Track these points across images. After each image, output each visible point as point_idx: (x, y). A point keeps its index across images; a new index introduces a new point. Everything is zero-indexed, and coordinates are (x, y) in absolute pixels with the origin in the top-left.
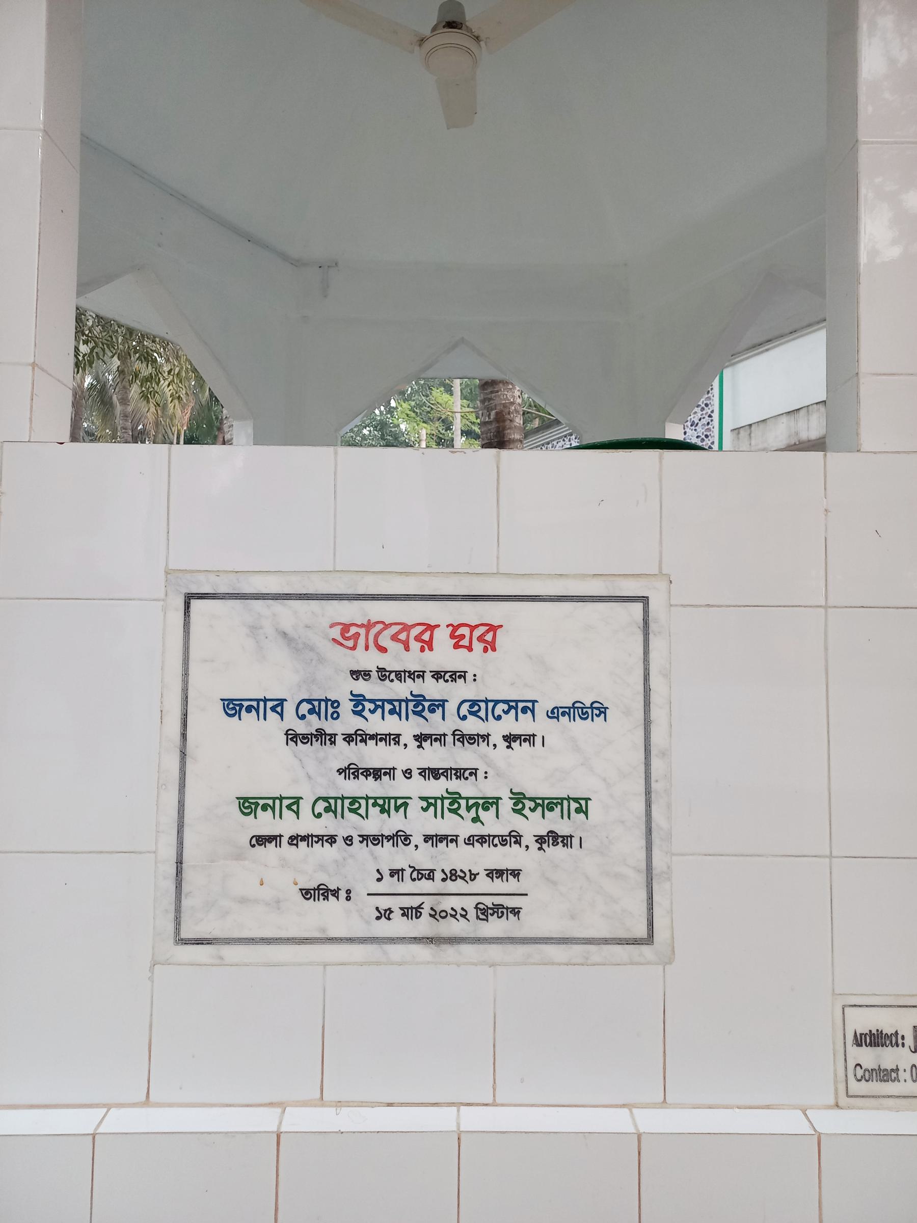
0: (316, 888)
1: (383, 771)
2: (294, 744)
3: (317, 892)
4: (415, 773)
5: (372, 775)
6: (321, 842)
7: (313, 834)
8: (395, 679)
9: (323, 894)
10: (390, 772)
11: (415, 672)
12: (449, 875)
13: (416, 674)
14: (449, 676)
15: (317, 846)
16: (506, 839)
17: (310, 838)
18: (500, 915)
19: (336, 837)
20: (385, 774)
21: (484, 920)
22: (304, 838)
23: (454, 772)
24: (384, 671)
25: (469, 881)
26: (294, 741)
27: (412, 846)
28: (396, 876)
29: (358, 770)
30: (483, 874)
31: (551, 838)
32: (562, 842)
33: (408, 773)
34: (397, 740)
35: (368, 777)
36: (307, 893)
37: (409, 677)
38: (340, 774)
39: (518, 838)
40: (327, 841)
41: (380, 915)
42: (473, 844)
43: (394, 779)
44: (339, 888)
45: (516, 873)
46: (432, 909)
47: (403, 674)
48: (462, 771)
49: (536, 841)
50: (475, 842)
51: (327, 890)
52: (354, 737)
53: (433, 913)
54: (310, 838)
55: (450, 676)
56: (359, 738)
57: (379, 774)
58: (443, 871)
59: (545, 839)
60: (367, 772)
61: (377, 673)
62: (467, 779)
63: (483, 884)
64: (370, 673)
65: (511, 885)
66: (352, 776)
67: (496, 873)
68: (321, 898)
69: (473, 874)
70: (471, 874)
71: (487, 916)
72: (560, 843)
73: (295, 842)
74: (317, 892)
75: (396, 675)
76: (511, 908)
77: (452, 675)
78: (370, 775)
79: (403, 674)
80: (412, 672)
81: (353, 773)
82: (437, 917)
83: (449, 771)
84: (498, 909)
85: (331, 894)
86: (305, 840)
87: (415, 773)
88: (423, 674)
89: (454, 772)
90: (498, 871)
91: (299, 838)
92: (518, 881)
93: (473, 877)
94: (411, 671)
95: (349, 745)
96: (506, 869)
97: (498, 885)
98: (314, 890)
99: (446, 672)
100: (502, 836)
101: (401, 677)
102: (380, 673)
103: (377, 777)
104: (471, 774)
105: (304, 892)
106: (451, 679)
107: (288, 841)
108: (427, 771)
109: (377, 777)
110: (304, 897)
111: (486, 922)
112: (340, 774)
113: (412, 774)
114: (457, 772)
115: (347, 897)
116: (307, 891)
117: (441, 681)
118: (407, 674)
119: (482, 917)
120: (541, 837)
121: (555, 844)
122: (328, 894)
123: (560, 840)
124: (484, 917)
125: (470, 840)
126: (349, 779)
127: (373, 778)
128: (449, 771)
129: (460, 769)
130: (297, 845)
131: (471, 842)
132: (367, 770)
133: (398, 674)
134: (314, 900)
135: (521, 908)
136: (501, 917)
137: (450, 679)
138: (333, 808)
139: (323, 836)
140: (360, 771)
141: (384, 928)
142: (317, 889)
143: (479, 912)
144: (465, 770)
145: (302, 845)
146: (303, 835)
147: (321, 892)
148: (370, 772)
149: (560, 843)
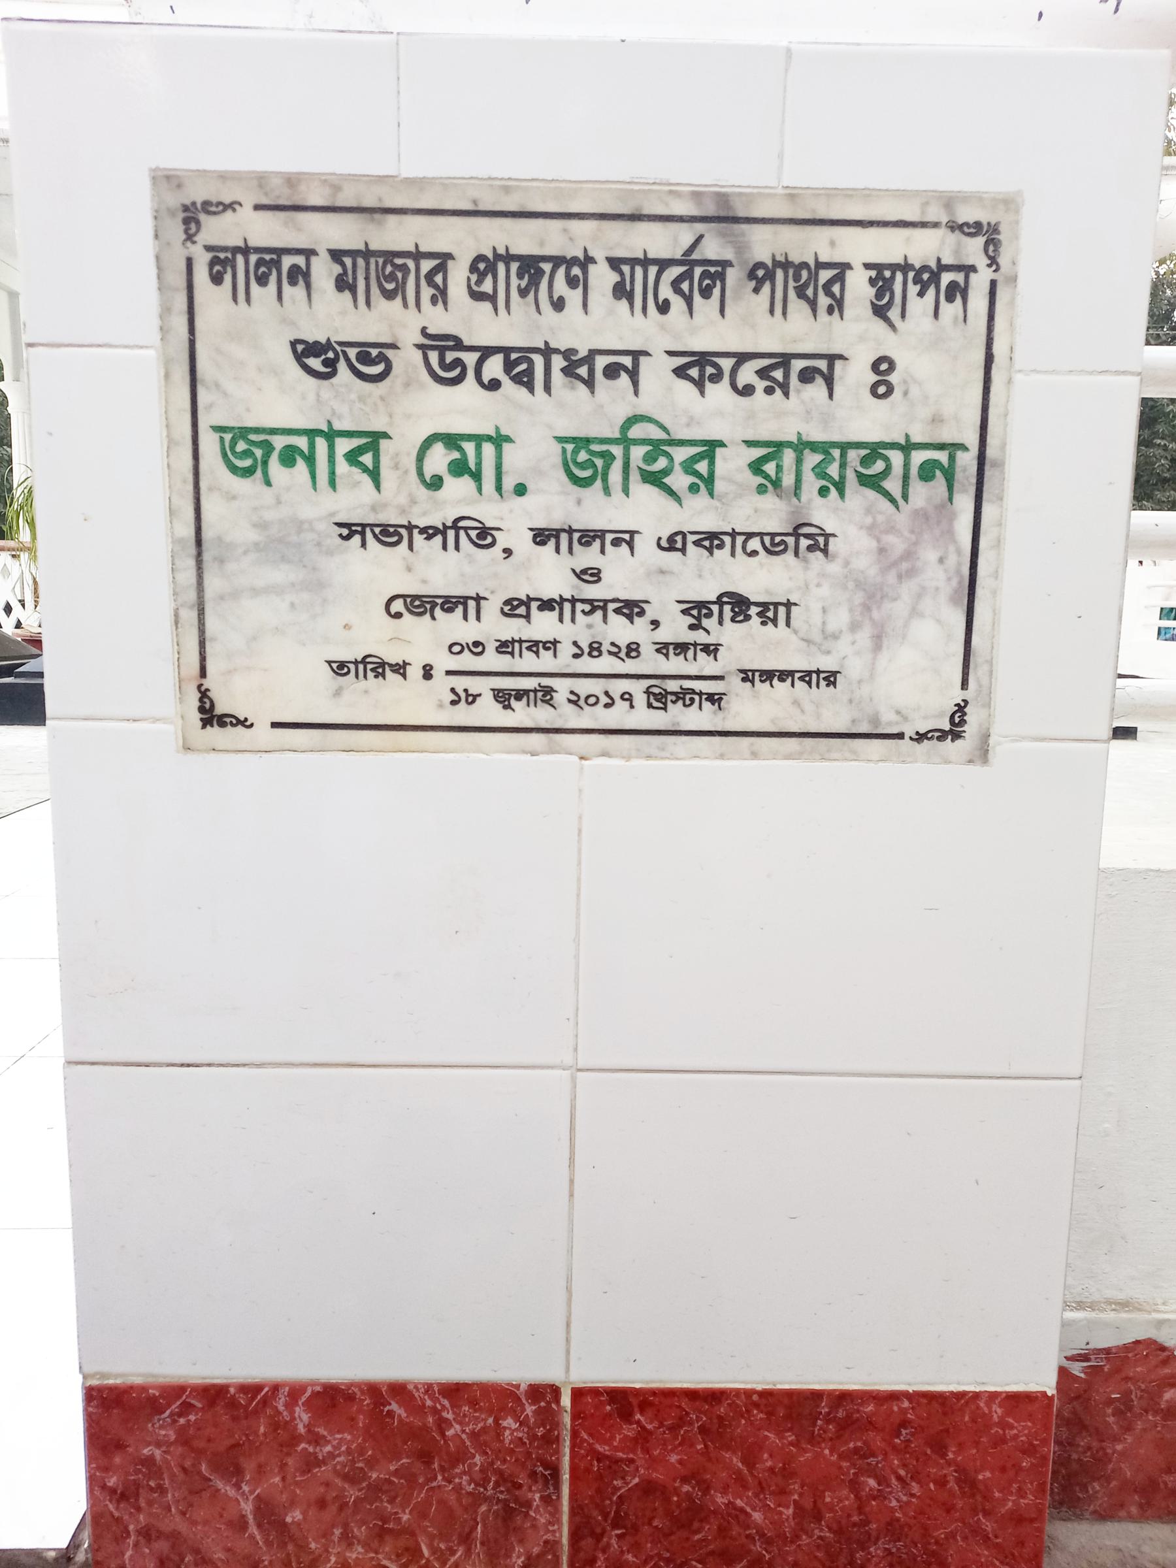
3: (361, 667)
11: (593, 353)
12: (587, 650)
13: (601, 362)
18: (688, 702)
19: (643, 605)
21: (661, 708)
25: (625, 658)
28: (525, 699)
31: (727, 608)
32: (759, 614)
41: (456, 699)
44: (407, 661)
46: (572, 692)
47: (538, 360)
51: (383, 664)
52: (790, 540)
53: (574, 698)
55: (763, 373)
56: (804, 543)
58: (575, 643)
63: (492, 660)
64: (390, 353)
65: (704, 664)
67: (675, 649)
68: (370, 674)
71: (665, 704)
74: (361, 667)
75: (509, 366)
76: (706, 694)
77: (772, 367)
79: (538, 360)
80: (583, 353)
82: (582, 703)
84: (685, 694)
91: (534, 605)
92: (716, 660)
96: (693, 643)
97: (675, 665)
98: (356, 663)
99: (742, 358)
101: (530, 372)
102: (434, 357)
105: (335, 666)
107: (502, 609)
111: (663, 711)
116: (342, 665)
118: (558, 362)
119: (656, 704)
120: (701, 605)
123: (754, 610)
130: (527, 617)
133: (517, 362)
134: (357, 676)
135: (724, 694)
136: (690, 705)
137: (760, 385)
138: (751, 678)
139: (606, 602)
141: (463, 715)
143: (652, 697)
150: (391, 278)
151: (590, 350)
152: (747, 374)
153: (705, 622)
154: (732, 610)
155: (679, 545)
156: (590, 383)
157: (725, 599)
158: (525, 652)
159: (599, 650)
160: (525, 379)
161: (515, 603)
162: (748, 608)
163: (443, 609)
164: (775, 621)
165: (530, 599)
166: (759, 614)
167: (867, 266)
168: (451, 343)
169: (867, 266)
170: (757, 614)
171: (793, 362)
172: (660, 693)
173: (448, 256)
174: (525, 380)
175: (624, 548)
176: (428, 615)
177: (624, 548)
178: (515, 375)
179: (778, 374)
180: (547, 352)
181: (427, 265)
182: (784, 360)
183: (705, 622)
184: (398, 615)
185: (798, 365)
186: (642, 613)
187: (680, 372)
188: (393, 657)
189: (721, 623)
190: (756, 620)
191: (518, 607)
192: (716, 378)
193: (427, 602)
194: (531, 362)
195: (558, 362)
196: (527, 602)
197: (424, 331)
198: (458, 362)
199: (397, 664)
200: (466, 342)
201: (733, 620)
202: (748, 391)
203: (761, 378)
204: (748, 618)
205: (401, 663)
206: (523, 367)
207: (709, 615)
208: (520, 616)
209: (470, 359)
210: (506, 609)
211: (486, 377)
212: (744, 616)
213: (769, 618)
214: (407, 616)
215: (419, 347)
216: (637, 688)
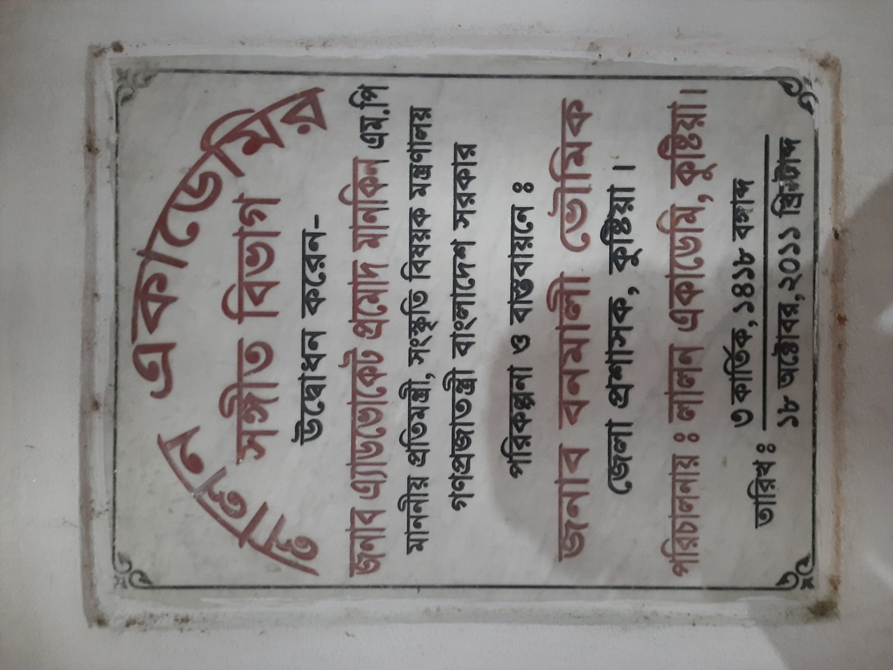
1: (515, 390)
2: (426, 267)
7: (607, 349)
8: (317, 401)
9: (765, 489)
12: (743, 299)
13: (308, 351)
15: (632, 340)
16: (682, 240)
20: (521, 386)
22: (615, 373)
24: (303, 427)
26: (422, 267)
27: (630, 301)
29: (513, 439)
30: (740, 243)
31: (616, 237)
32: (622, 211)
34: (421, 113)
36: (763, 517)
37: (314, 367)
38: (520, 472)
39: (678, 213)
42: (695, 313)
43: (530, 369)
49: (687, 183)
50: (688, 307)
51: (759, 482)
54: (616, 357)
55: (313, 269)
57: (522, 397)
62: (530, 226)
66: (525, 449)
67: (740, 221)
68: (770, 491)
70: (786, 409)
72: (692, 131)
73: (621, 392)
75: (311, 398)
78: (522, 415)
80: (304, 360)
83: (516, 260)
86: (619, 369)
90: (736, 219)
91: (615, 381)
93: (746, 259)
94: (303, 365)
95: (429, 216)
99: (305, 280)
100: (673, 248)
101: (314, 387)
102: (306, 436)
104: (522, 218)
105: (760, 521)
106: (318, 267)
108: (516, 306)
112: (520, 472)
113: (520, 334)
115: (769, 450)
116: (759, 515)
117: (323, 291)
118: (309, 373)
123: (618, 216)
125: (683, 318)
127: (528, 408)
128: (516, 260)
129: (513, 237)
130: (628, 388)
131: (689, 316)
132: (513, 421)
134: (774, 503)
137: (319, 270)
144: (514, 228)
145: (628, 375)
147: (761, 492)
148: (518, 414)
149: (692, 131)
150: (367, 565)
152: (314, 277)
154: (618, 233)
155: (157, 357)
157: (608, 238)
159: (743, 288)
160: (318, 390)
161: (614, 397)
162: (617, 221)
163: (623, 451)
164: (628, 200)
165: (610, 385)
168: (300, 428)
170: (621, 213)
172: (781, 201)
173: (353, 511)
174: (318, 390)
176: (628, 463)
178: (315, 393)
179: (314, 261)
180: (303, 378)
181: (359, 524)
182: (306, 259)
184: (629, 485)
185: (309, 252)
186: (622, 301)
188: (753, 474)
189: (630, 241)
190: (628, 214)
192: (316, 292)
193: (615, 463)
194: (309, 386)
195: (309, 373)
197: (294, 440)
198: (310, 423)
199: (758, 469)
200: (299, 419)
201: (627, 232)
202: (322, 277)
203: (316, 269)
204: (625, 220)
205: (756, 466)
206: (311, 391)
207: (623, 250)
209: (308, 418)
210: (619, 403)
211: (317, 409)
212: (624, 223)
213: (625, 205)
214: (628, 478)
215: (302, 443)
216: (777, 225)
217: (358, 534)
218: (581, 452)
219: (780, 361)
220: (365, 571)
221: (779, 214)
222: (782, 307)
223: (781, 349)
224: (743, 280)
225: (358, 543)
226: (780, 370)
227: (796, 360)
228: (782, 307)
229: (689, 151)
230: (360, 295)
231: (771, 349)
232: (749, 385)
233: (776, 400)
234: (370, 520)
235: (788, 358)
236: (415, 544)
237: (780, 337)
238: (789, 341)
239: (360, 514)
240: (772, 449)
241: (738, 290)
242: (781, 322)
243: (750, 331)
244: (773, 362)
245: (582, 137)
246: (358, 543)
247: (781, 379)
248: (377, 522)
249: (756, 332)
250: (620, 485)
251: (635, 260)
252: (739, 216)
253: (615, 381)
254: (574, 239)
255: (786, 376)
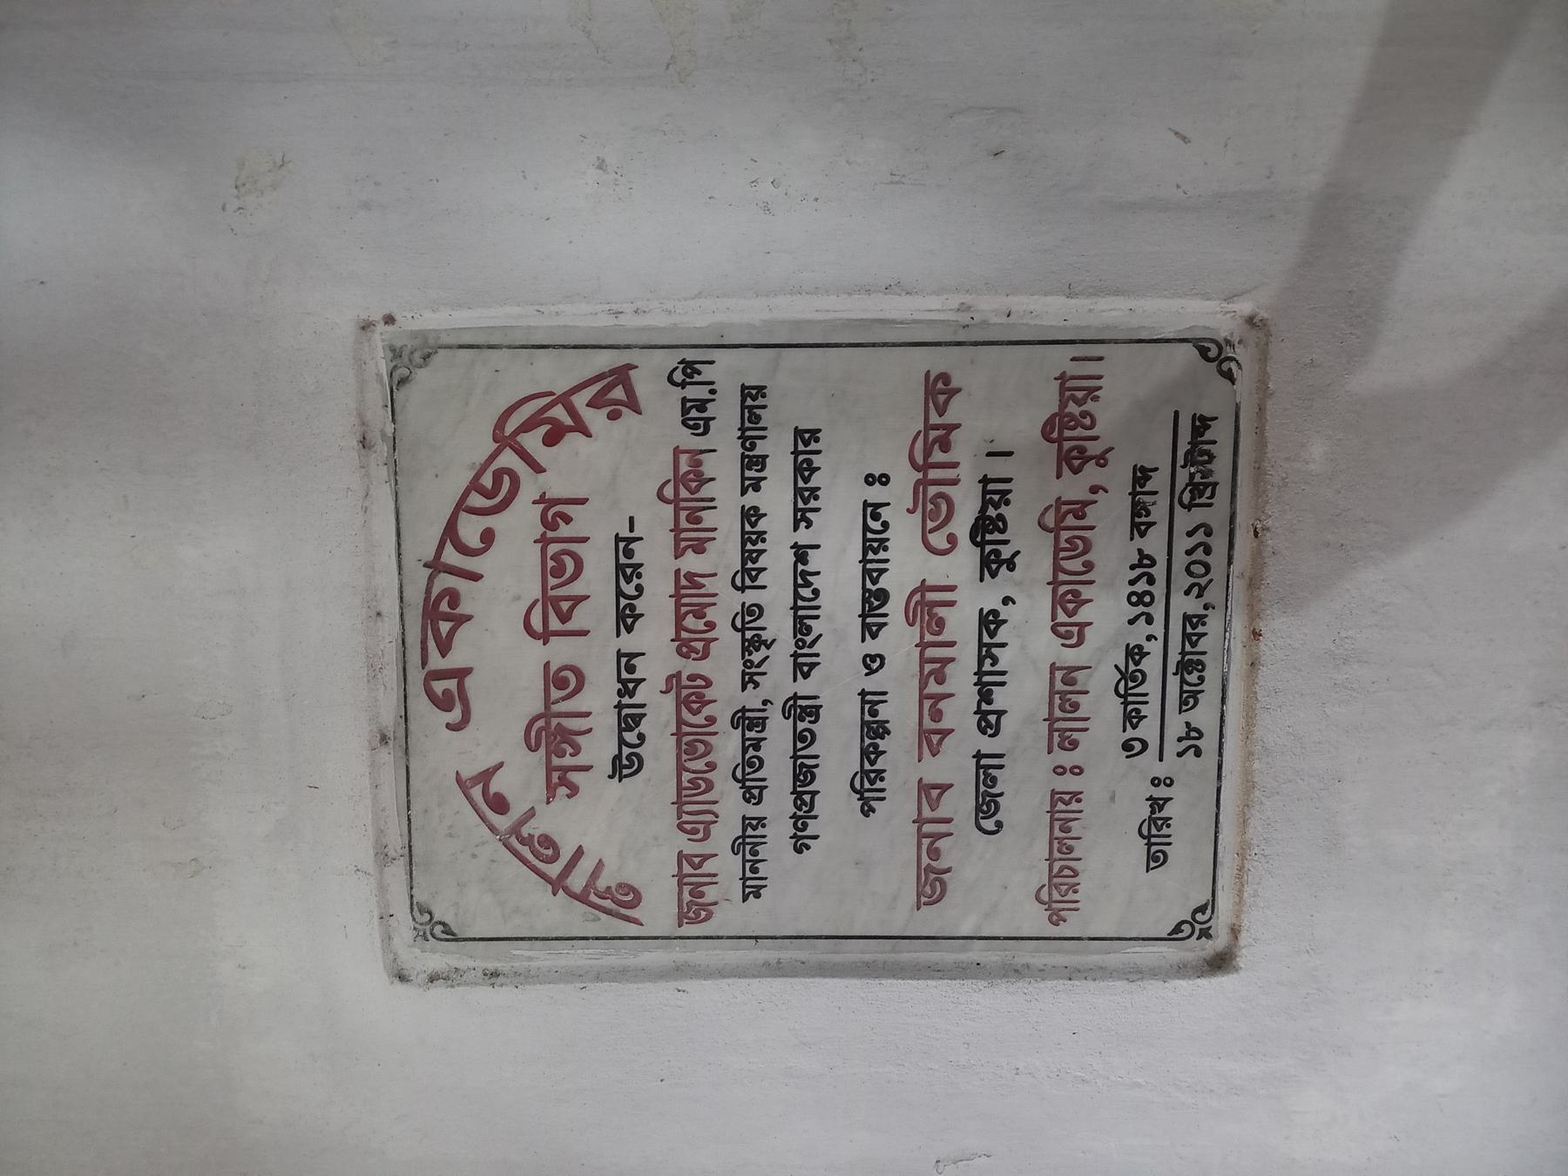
0: (1146, 841)
1: (867, 717)
3: (1153, 840)
4: (872, 647)
5: (878, 741)
6: (994, 650)
10: (870, 702)
11: (619, 680)
12: (1141, 609)
13: (625, 675)
14: (628, 583)
15: (1005, 658)
17: (986, 679)
20: (874, 713)
23: (871, 556)
24: (621, 761)
27: (1005, 613)
31: (988, 537)
32: (996, 507)
33: (873, 663)
35: (814, 465)
36: (1156, 859)
37: (632, 694)
39: (1064, 508)
40: (992, 635)
42: (1082, 626)
43: (885, 693)
45: (1142, 475)
47: (625, 711)
48: (869, 535)
49: (1076, 471)
51: (1152, 820)
53: (1195, 590)
54: (986, 679)
57: (875, 726)
59: (1132, 711)
60: (870, 753)
61: (624, 780)
68: (1165, 831)
69: (1188, 733)
72: (1084, 408)
73: (992, 718)
74: (1153, 840)
77: (625, 575)
78: (876, 746)
79: (625, 711)
80: (620, 686)
81: (872, 782)
83: (869, 566)
85: (1159, 812)
86: (991, 692)
87: (872, 647)
88: (626, 655)
89: (871, 556)
90: (1135, 514)
91: (984, 707)
92: (1156, 469)
94: (619, 690)
99: (620, 593)
101: (632, 716)
102: (625, 772)
103: (881, 730)
104: (876, 517)
105: (1152, 864)
108: (869, 620)
109: (881, 730)
110: (1162, 865)
114: (871, 547)
115: (1165, 784)
118: (626, 700)
121: (1000, 524)
122: (1160, 819)
123: (992, 512)
124: (1208, 493)
126: (883, 790)
127: (883, 738)
128: (869, 566)
129: (865, 540)
130: (1000, 713)
132: (864, 753)
137: (636, 581)
140: (867, 766)
142: (1149, 840)
144: (866, 528)
145: (1000, 698)
146: (978, 698)
148: (870, 745)
149: (1084, 408)
151: (618, 682)
153: (1006, 555)
156: (639, 681)
157: (979, 539)
158: (1198, 649)
159: (1140, 596)
162: (990, 518)
166: (996, 507)
167: (796, 528)
169: (796, 528)
171: (621, 562)
174: (637, 719)
175: (497, 785)
177: (497, 785)
181: (687, 869)
182: (619, 568)
183: (1006, 555)
185: (623, 560)
186: (995, 613)
187: (629, 629)
188: (1145, 811)
191: (988, 722)
192: (632, 607)
194: (627, 715)
195: (626, 700)
196: (982, 714)
198: (628, 758)
201: (1002, 531)
204: (1001, 517)
207: (997, 553)
208: (998, 720)
209: (626, 751)
210: (990, 732)
216: (1184, 521)
217: (686, 880)
218: (944, 788)
219: (1183, 681)
220: (696, 920)
221: (1189, 507)
222: (1187, 618)
223: (1184, 667)
224: (1141, 586)
225: (686, 889)
226: (1182, 692)
227: (1201, 679)
228: (1187, 618)
229: (1079, 432)
230: (684, 609)
231: (1172, 668)
232: (1144, 710)
233: (1176, 726)
234: (700, 866)
235: (1193, 678)
236: (752, 890)
237: (1183, 653)
238: (1195, 657)
239: (689, 858)
240: (1169, 782)
241: (1134, 599)
242: (1186, 636)
243: (1148, 646)
244: (1173, 683)
245: (949, 418)
246: (686, 889)
247: (1183, 702)
248: (708, 867)
249: (1155, 648)
250: (989, 824)
251: (1011, 565)
252: (1138, 509)
253: (984, 707)
254: (939, 540)
255: (1189, 699)
